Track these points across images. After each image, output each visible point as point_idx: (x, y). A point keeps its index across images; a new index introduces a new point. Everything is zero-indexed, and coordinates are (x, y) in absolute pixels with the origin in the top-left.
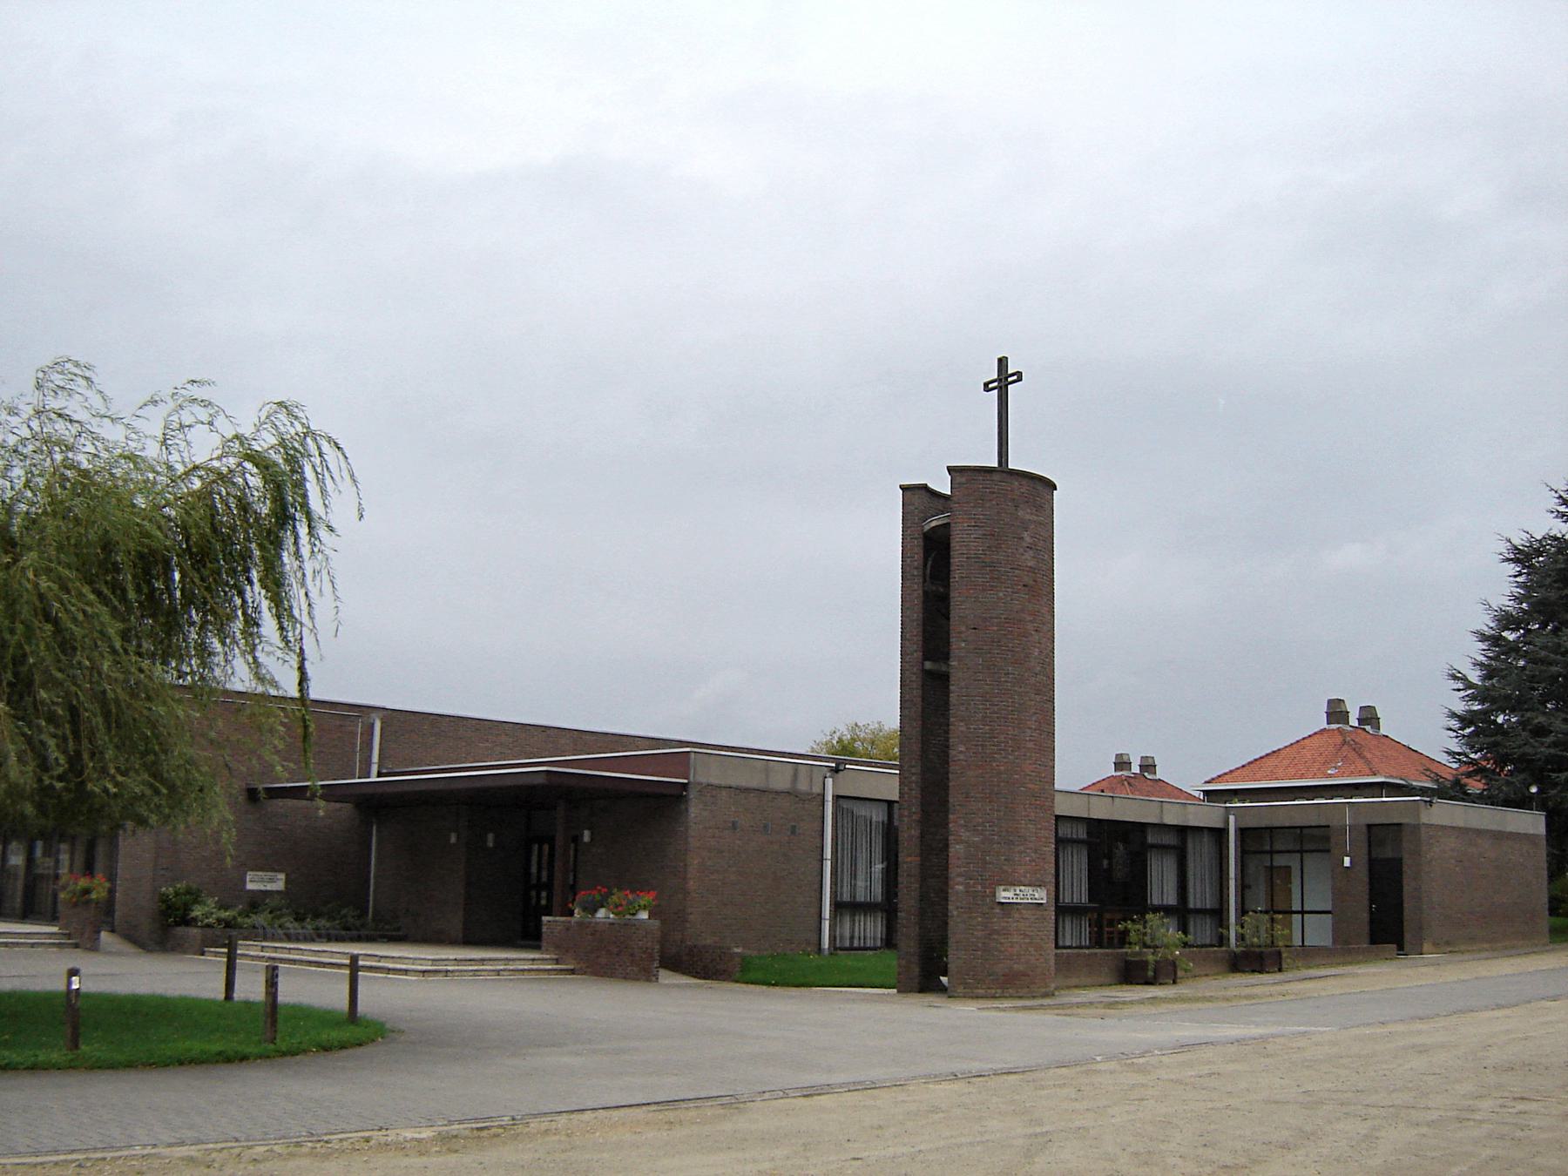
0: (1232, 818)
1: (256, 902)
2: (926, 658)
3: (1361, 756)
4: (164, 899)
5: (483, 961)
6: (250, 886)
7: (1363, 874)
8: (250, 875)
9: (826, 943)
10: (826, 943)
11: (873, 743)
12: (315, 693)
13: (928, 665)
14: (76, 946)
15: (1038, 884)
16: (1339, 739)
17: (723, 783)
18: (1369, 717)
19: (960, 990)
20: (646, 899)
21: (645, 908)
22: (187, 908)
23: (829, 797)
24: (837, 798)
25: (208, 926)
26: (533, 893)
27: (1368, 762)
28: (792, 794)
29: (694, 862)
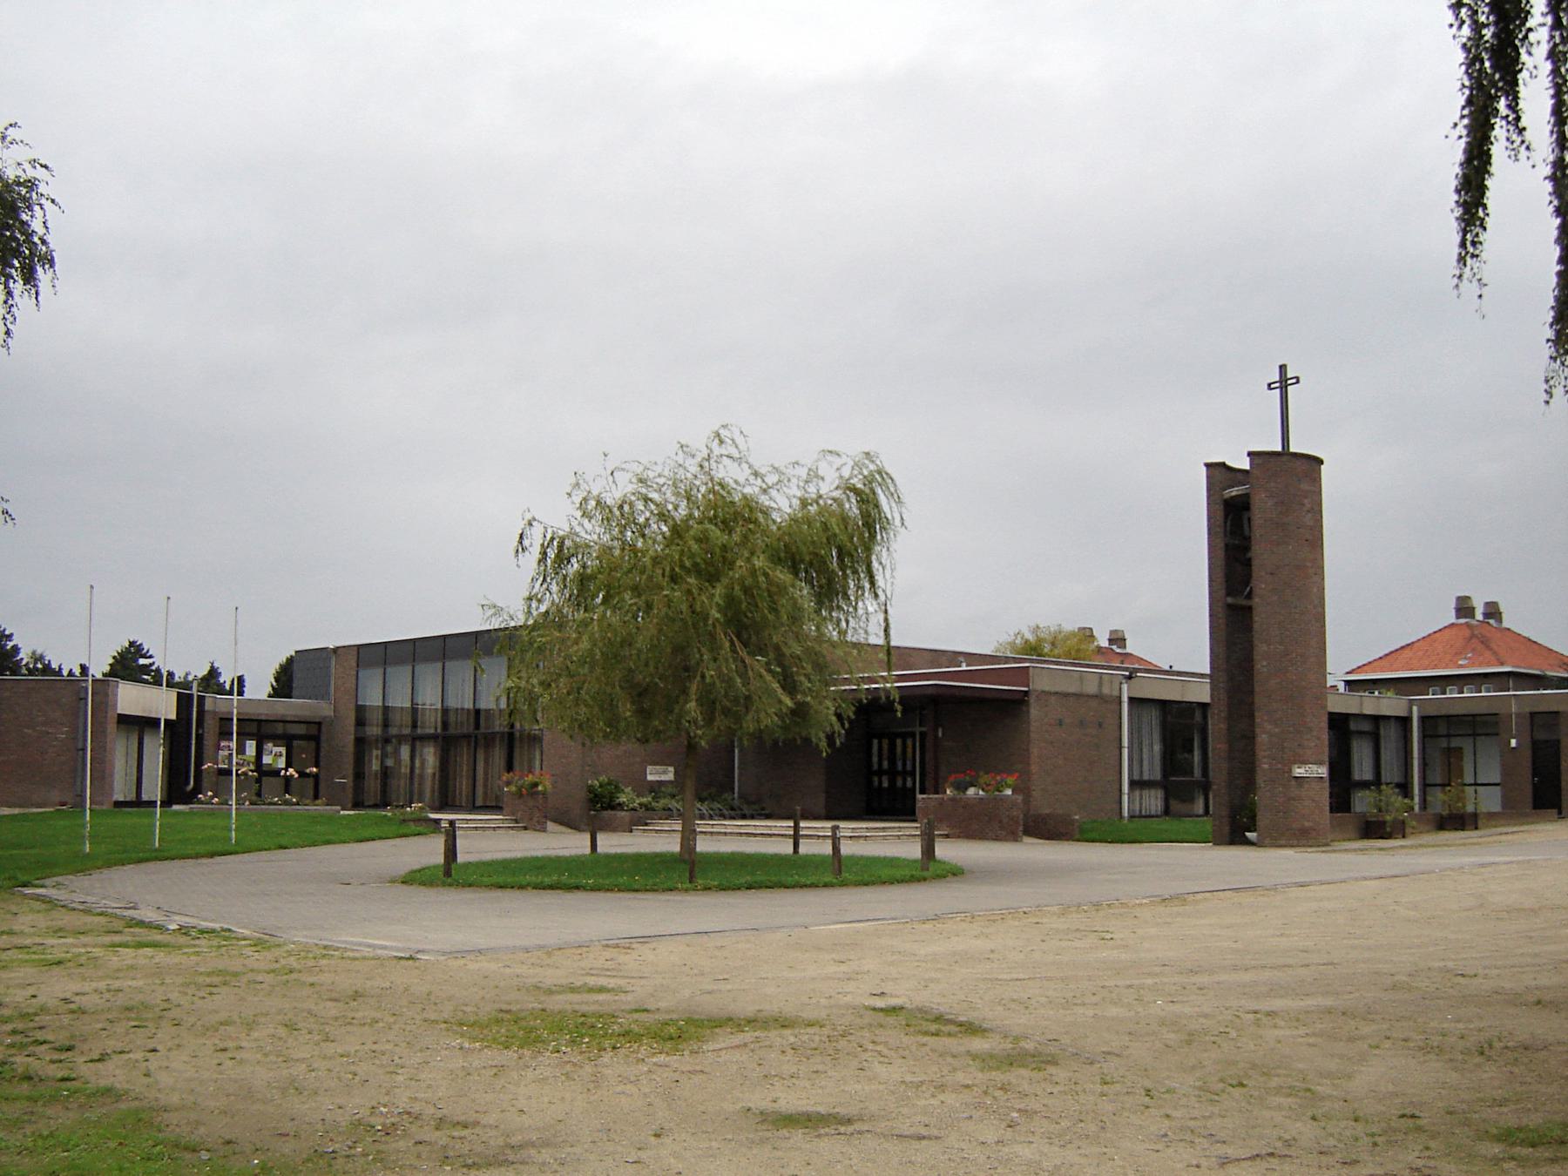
0: (1415, 708)
1: (656, 789)
2: (1228, 594)
3: (1488, 648)
4: (591, 789)
5: (884, 829)
6: (650, 778)
7: (1527, 754)
8: (649, 768)
9: (1126, 814)
10: (1126, 814)
11: (1053, 644)
12: (893, 643)
13: (1230, 600)
14: (525, 828)
15: (1320, 763)
16: (1467, 633)
17: (1053, 690)
18: (1493, 611)
19: (1267, 841)
20: (1010, 780)
21: (1009, 786)
22: (612, 797)
23: (1125, 699)
24: (1131, 699)
25: (634, 809)
26: (876, 779)
27: (1495, 653)
28: (1098, 697)
29: (1035, 751)
